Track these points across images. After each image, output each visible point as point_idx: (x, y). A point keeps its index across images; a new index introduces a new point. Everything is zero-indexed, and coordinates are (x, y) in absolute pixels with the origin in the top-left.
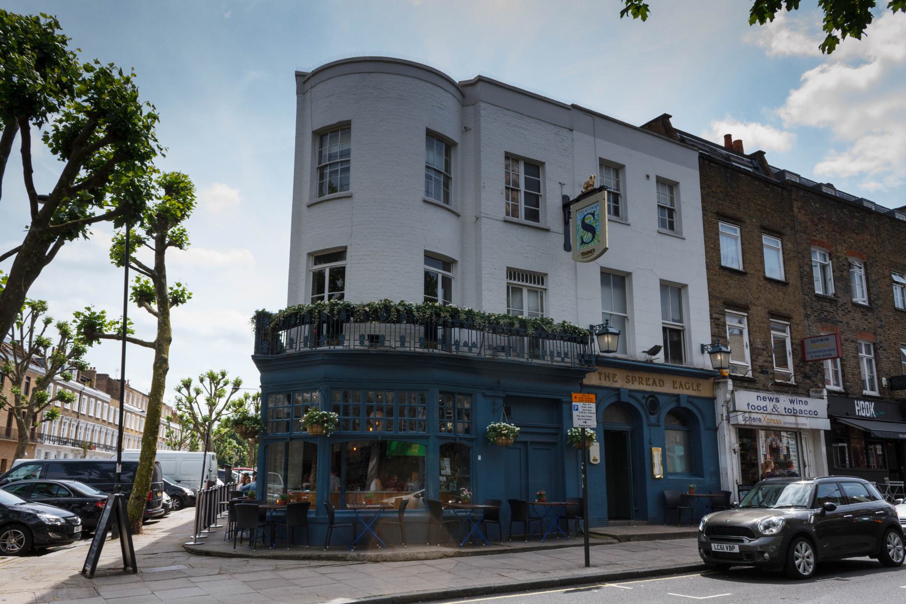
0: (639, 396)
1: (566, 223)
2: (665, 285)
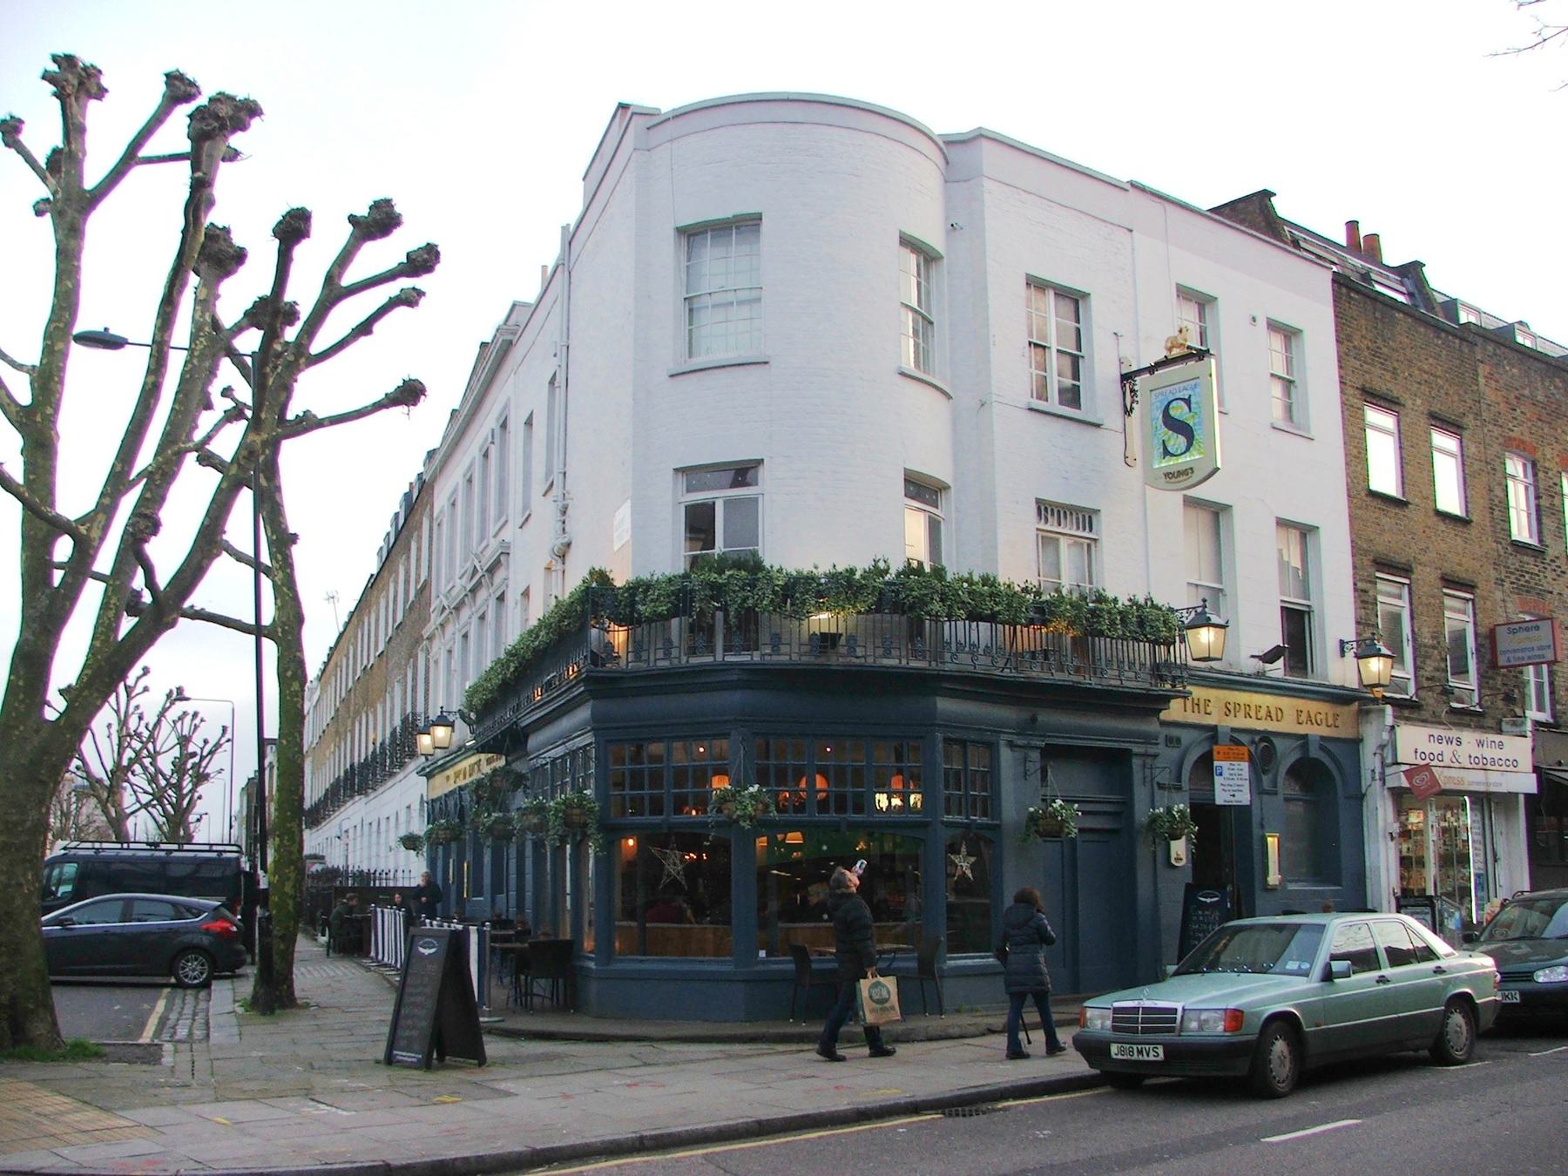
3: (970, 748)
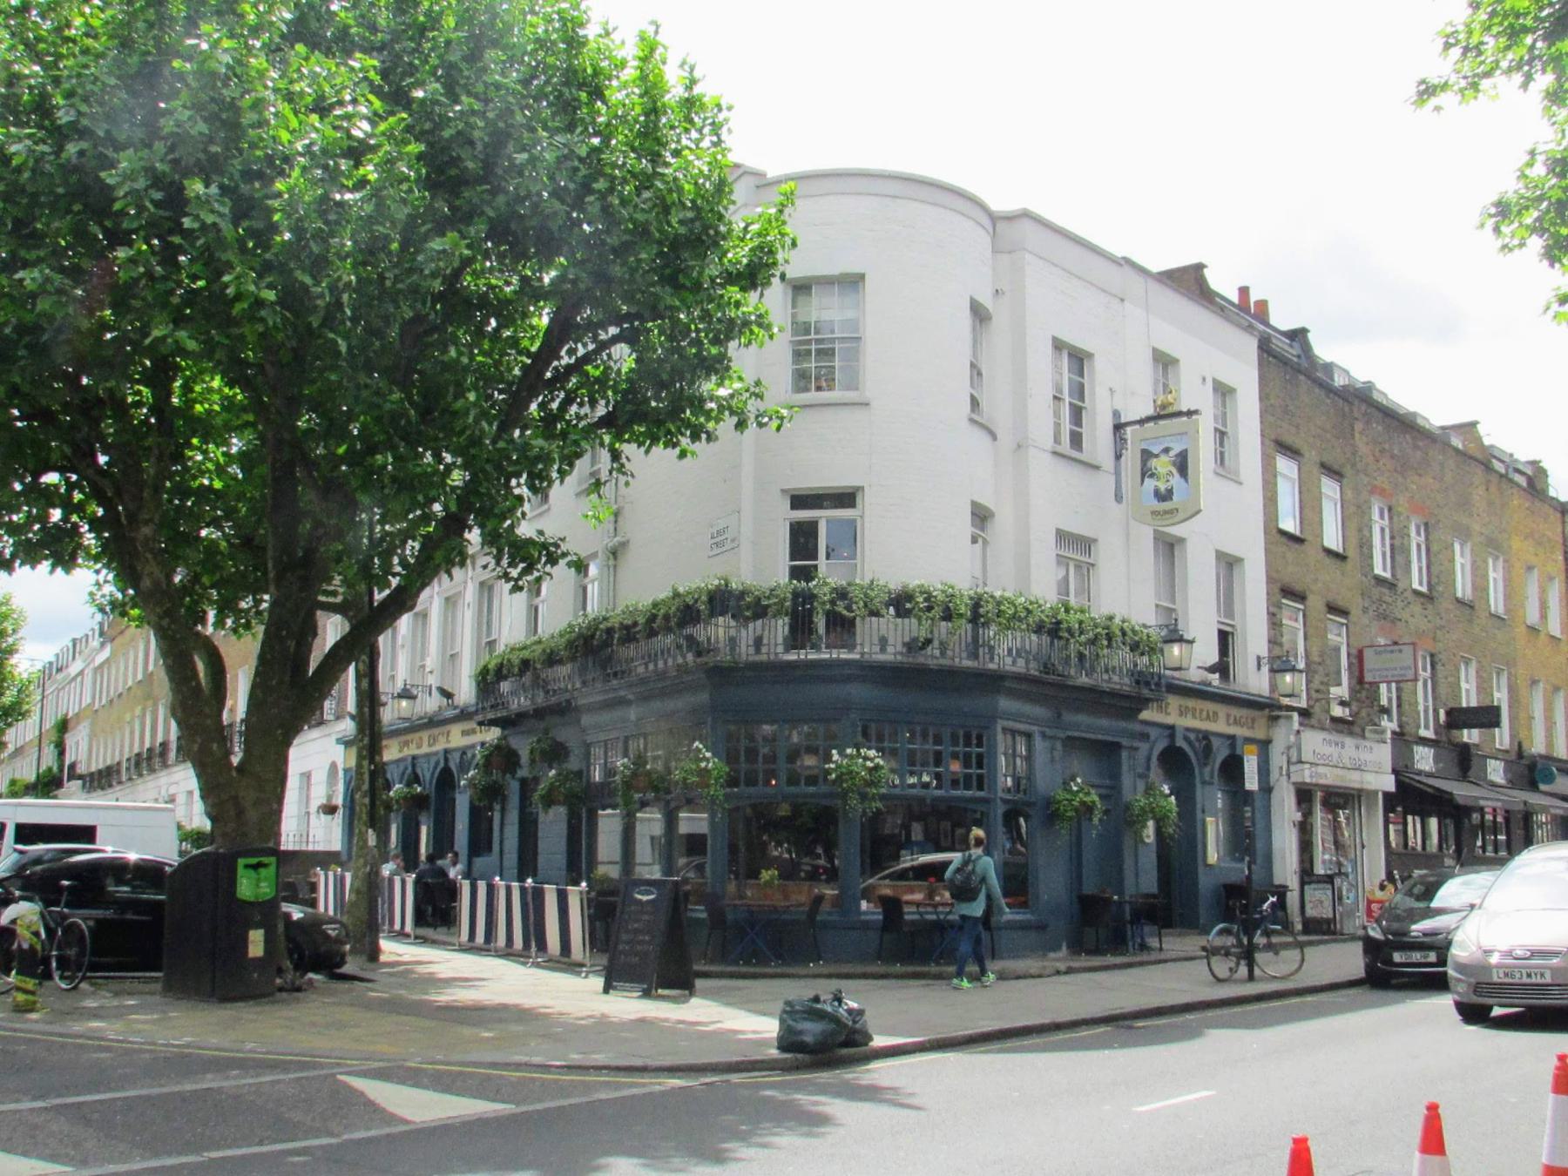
0: (1192, 736)
1: (1118, 457)
2: (1220, 555)
3: (1018, 738)
